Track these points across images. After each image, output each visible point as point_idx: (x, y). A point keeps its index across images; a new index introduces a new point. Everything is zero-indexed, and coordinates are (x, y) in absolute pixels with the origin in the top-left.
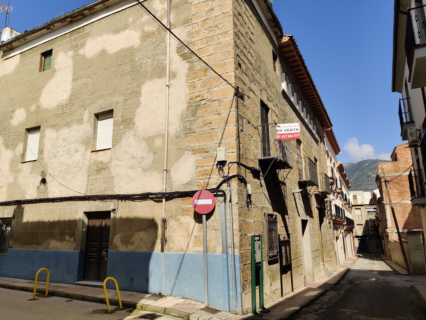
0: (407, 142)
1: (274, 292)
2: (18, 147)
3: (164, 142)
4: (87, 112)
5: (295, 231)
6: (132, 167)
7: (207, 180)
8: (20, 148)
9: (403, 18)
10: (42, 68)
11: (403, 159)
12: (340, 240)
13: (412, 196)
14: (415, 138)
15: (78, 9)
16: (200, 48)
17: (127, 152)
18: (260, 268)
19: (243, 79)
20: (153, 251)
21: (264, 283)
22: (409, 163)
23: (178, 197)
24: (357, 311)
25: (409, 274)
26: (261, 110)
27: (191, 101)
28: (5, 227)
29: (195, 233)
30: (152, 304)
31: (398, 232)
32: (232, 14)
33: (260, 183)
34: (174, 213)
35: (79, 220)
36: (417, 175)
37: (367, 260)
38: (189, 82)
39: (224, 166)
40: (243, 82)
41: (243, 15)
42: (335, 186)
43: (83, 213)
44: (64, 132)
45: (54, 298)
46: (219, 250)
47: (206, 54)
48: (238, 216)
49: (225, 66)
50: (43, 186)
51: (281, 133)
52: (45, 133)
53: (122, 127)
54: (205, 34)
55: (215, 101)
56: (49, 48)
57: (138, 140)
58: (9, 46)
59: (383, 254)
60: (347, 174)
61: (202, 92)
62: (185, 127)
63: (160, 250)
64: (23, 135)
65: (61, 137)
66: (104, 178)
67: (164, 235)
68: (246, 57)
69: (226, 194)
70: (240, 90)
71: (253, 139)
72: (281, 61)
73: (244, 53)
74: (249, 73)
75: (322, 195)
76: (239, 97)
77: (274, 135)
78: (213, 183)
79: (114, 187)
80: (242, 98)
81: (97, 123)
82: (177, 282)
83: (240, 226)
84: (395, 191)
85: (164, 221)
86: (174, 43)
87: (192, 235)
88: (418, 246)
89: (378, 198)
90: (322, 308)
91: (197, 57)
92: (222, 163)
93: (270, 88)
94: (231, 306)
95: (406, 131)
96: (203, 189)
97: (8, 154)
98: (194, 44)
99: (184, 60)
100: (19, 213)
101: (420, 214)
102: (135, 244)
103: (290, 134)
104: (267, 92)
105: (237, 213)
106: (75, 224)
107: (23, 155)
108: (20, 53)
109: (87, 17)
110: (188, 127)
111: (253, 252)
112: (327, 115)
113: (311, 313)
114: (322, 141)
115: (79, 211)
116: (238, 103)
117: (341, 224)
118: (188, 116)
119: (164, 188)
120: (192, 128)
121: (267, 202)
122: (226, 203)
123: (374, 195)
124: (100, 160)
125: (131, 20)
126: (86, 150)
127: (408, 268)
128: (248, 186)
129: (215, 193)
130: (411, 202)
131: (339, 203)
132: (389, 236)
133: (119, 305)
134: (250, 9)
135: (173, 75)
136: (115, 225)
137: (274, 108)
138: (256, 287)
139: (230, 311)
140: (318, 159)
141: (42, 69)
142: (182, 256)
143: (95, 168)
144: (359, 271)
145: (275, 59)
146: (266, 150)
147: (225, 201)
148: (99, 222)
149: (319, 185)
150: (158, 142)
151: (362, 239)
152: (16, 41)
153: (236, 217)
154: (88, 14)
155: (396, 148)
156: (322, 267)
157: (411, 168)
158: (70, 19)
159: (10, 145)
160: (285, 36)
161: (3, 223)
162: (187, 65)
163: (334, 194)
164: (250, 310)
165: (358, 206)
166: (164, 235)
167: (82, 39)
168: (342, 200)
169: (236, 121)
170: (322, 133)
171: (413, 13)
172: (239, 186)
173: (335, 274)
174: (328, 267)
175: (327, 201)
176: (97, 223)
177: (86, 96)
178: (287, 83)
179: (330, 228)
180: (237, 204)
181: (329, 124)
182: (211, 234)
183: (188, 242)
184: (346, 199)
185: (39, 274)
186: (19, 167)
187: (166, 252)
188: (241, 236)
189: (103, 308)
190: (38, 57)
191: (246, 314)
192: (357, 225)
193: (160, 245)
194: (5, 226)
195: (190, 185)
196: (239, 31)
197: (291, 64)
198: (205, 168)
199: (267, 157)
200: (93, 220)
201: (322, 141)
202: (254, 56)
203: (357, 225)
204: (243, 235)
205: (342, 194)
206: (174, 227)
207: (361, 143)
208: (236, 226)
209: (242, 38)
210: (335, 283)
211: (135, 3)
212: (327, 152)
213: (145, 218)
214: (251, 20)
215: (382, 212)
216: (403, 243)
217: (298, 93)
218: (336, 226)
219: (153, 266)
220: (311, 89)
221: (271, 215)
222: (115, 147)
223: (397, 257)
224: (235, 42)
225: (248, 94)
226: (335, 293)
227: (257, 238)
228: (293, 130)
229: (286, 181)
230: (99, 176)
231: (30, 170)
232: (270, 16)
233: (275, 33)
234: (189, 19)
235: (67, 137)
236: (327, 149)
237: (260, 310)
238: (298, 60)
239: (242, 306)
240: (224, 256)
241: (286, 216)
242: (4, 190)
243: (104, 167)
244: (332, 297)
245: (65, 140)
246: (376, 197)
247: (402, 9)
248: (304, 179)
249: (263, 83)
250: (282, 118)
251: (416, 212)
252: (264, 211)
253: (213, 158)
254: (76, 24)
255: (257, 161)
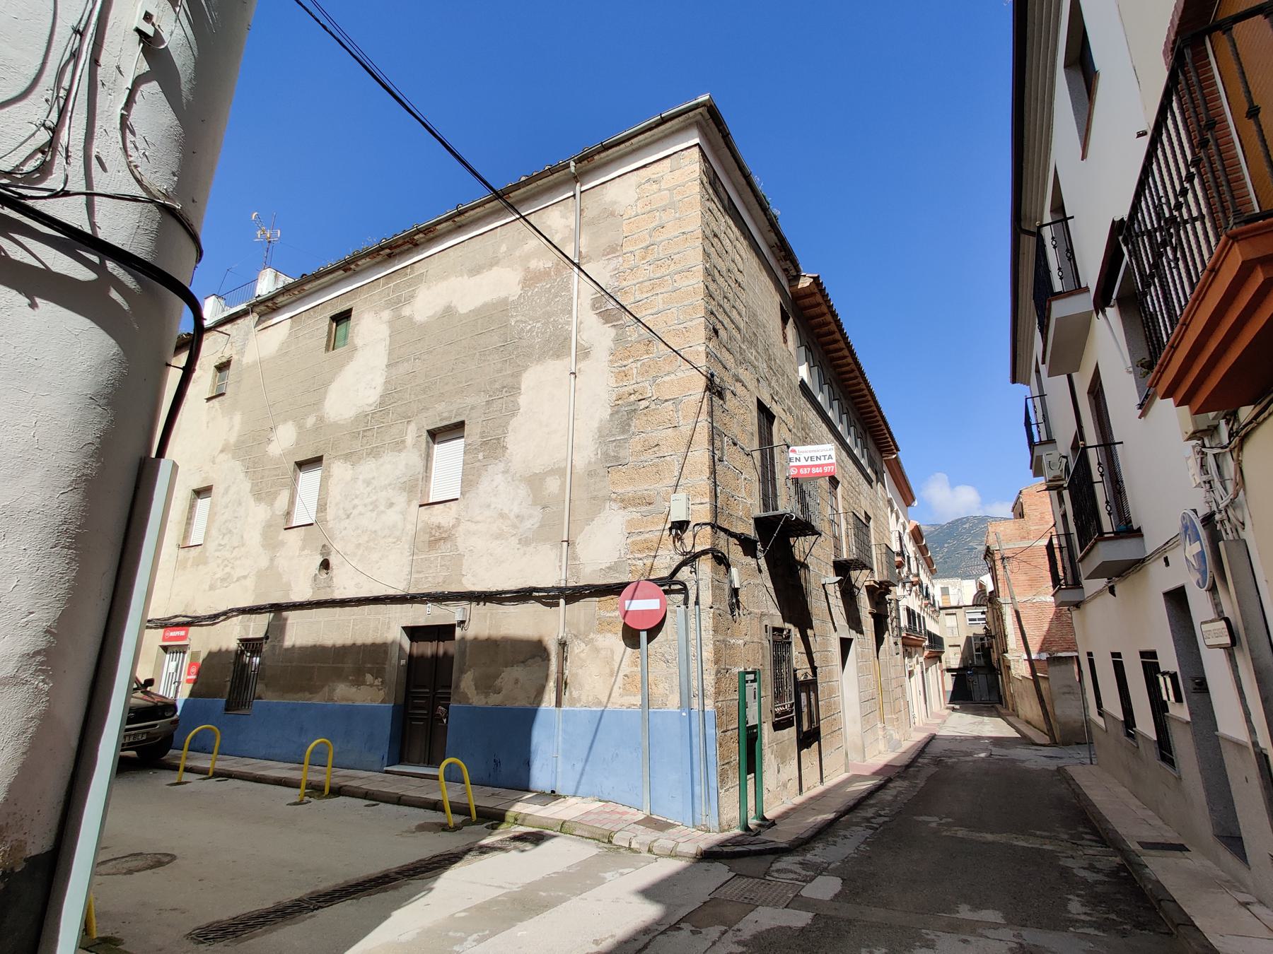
0: (1042, 480)
1: (785, 785)
2: (279, 498)
3: (563, 483)
4: (412, 428)
5: (827, 661)
6: (499, 536)
7: (651, 560)
8: (284, 497)
9: (1029, 243)
10: (331, 344)
11: (1036, 514)
12: (917, 677)
13: (1054, 587)
14: (1058, 473)
15: (404, 231)
16: (638, 299)
17: (489, 506)
18: (756, 738)
19: (721, 358)
20: (539, 705)
21: (764, 768)
22: (1047, 523)
23: (591, 595)
24: (950, 820)
25: (1054, 743)
26: (759, 420)
27: (620, 402)
28: (250, 657)
29: (626, 669)
30: (537, 812)
31: (1030, 660)
32: (700, 236)
33: (758, 565)
34: (582, 628)
35: (393, 642)
36: (1064, 544)
37: (970, 716)
38: (616, 365)
39: (684, 531)
40: (722, 364)
41: (722, 236)
42: (906, 569)
43: (400, 629)
44: (368, 468)
45: (341, 799)
46: (674, 702)
47: (649, 312)
48: (711, 633)
49: (687, 335)
50: (324, 575)
51: (798, 463)
52: (332, 470)
53: (480, 456)
54: (646, 272)
55: (666, 401)
56: (345, 307)
57: (513, 481)
58: (270, 304)
59: (1001, 703)
60: (928, 545)
61: (641, 385)
62: (606, 454)
63: (554, 703)
64: (290, 473)
65: (361, 477)
66: (443, 557)
67: (561, 672)
68: (729, 317)
69: (689, 588)
70: (717, 380)
71: (743, 477)
72: (798, 323)
73: (724, 309)
74: (734, 347)
75: (881, 588)
76: (714, 393)
77: (786, 468)
78: (662, 566)
79: (463, 575)
80: (720, 395)
81: (433, 448)
82: (587, 768)
83: (717, 652)
84: (1023, 578)
85: (563, 644)
86: (588, 290)
87: (618, 672)
88: (1070, 686)
89: (991, 593)
90: (880, 816)
91: (632, 318)
92: (681, 526)
93: (775, 375)
94: (697, 816)
95: (1040, 459)
96: (642, 578)
97: (259, 514)
98: (626, 293)
99: (607, 322)
100: (276, 629)
101: (1072, 623)
102: (504, 692)
103: (818, 466)
104: (769, 384)
105: (711, 625)
106: (385, 651)
107: (288, 514)
108: (291, 317)
109: (422, 247)
110: (612, 454)
111: (743, 705)
112: (888, 429)
113: (857, 824)
114: (880, 479)
115: (392, 624)
116: (712, 406)
117: (918, 645)
118: (613, 433)
119: (564, 577)
120: (621, 455)
121: (770, 603)
122: (687, 607)
123: (982, 587)
124: (436, 523)
125: (504, 248)
126: (409, 502)
127: (1050, 732)
128: (734, 570)
129: (667, 588)
130: (1053, 599)
131: (915, 603)
132: (1012, 667)
133: (470, 815)
134: (736, 226)
135: (584, 353)
136: (463, 653)
137: (783, 416)
138: (749, 776)
139: (694, 826)
140: (872, 516)
141: (332, 347)
142: (599, 714)
143: (427, 537)
144: (953, 739)
145: (785, 320)
146: (768, 497)
147: (686, 602)
148: (432, 648)
149: (875, 568)
150: (553, 485)
151: (960, 676)
152: (283, 293)
153: (708, 635)
154: (422, 240)
155: (1021, 492)
156: (881, 733)
157: (1051, 530)
158: (388, 251)
159: (264, 495)
160: (805, 276)
161: (246, 648)
162: (612, 333)
163: (904, 586)
164: (736, 823)
165: (950, 609)
166: (561, 672)
167: (410, 286)
168: (921, 596)
169: (709, 442)
170: (879, 464)
171: (1047, 233)
172: (714, 571)
173: (906, 745)
174: (892, 732)
175: (891, 600)
176: (428, 648)
177: (413, 396)
178: (810, 367)
179: (897, 654)
180: (711, 608)
181: (893, 447)
182: (657, 669)
183: (610, 687)
184: (927, 596)
185: (312, 752)
186: (280, 538)
187: (565, 708)
188: (718, 672)
189: (436, 821)
190: (324, 324)
191: (728, 830)
192: (950, 646)
193: (555, 693)
194: (249, 654)
195: (614, 570)
196: (715, 266)
197: (817, 330)
198: (647, 536)
199: (771, 513)
200: (421, 643)
201: (880, 479)
202: (744, 313)
203: (950, 646)
204: (722, 671)
205: (921, 586)
206: (583, 655)
207: (953, 484)
208: (708, 653)
209: (720, 280)
210: (907, 763)
211: (514, 218)
212: (890, 501)
213: (525, 639)
214: (738, 245)
215: (998, 619)
216: (1040, 680)
217: (830, 385)
218: (909, 649)
219: (539, 736)
220: (856, 377)
221: (778, 630)
222: (467, 495)
223: (1028, 708)
224: (707, 287)
225: (732, 388)
226: (906, 783)
227: (751, 677)
228: (822, 458)
229: (809, 561)
230: (433, 555)
231: (300, 543)
232: (775, 238)
233: (785, 270)
234: (617, 245)
235: (373, 478)
236: (890, 496)
237: (755, 821)
238: (830, 323)
239: (719, 816)
240: (684, 714)
241: (809, 632)
242: (250, 583)
243: (443, 535)
244: (900, 793)
245: (368, 483)
246: (985, 590)
247: (1025, 226)
248: (845, 557)
249: (763, 366)
250: (799, 435)
251: (1064, 619)
252: (766, 622)
253: (663, 516)
254: (399, 261)
255: (752, 521)
